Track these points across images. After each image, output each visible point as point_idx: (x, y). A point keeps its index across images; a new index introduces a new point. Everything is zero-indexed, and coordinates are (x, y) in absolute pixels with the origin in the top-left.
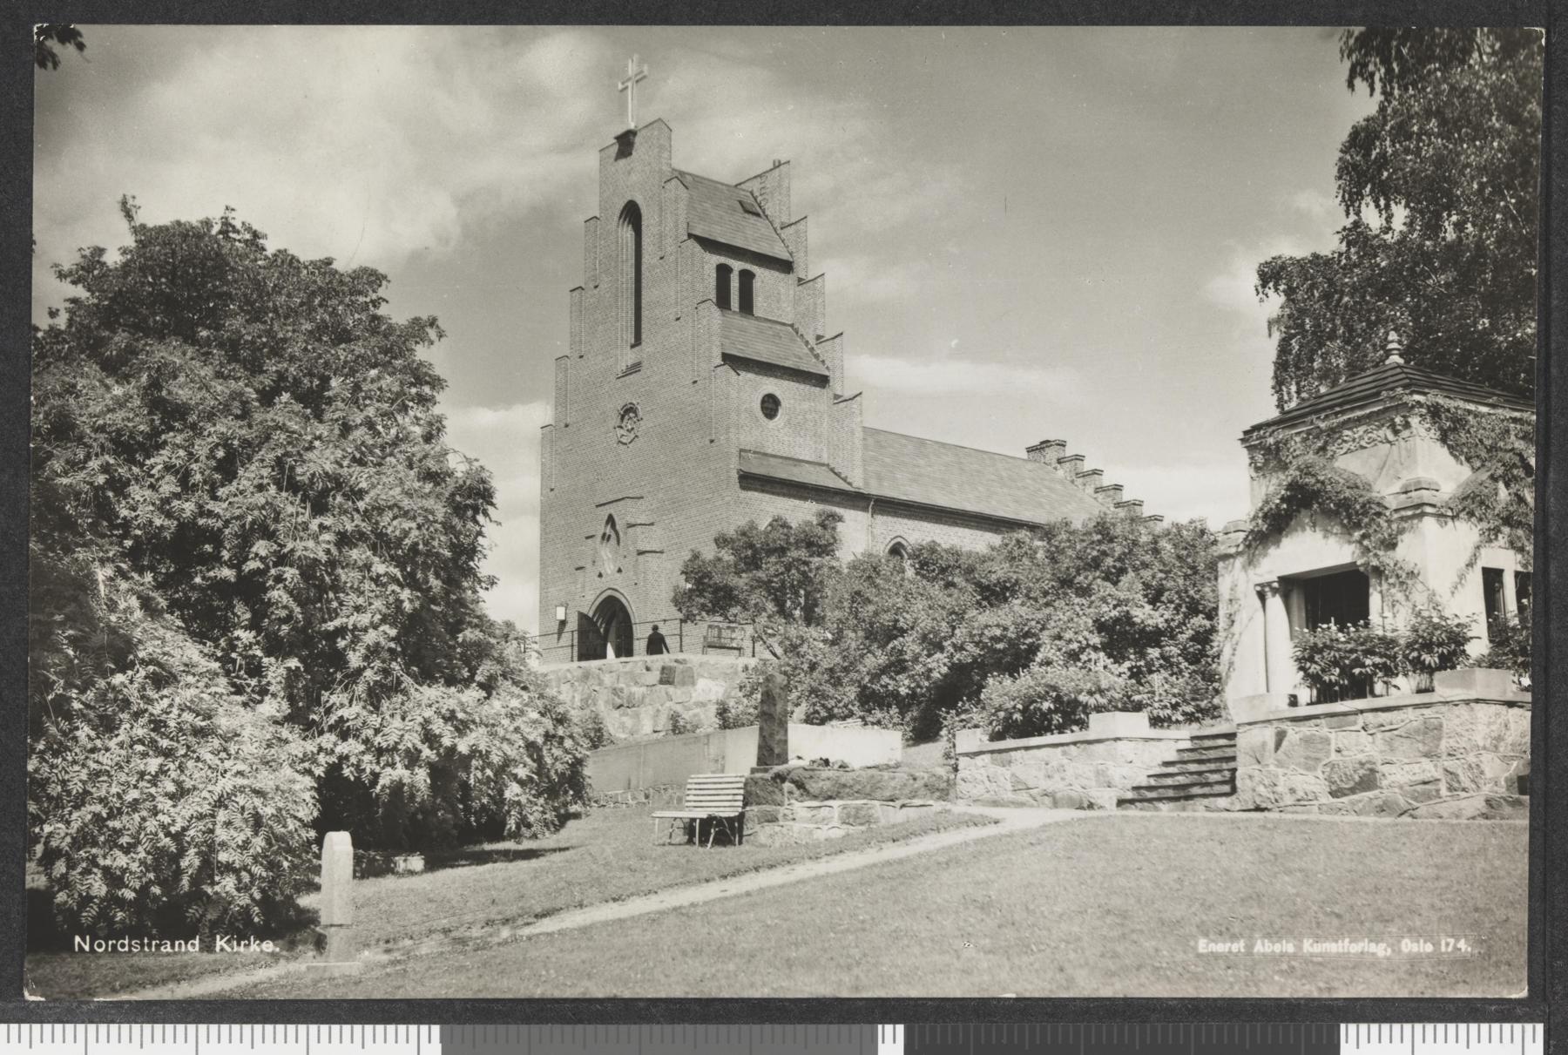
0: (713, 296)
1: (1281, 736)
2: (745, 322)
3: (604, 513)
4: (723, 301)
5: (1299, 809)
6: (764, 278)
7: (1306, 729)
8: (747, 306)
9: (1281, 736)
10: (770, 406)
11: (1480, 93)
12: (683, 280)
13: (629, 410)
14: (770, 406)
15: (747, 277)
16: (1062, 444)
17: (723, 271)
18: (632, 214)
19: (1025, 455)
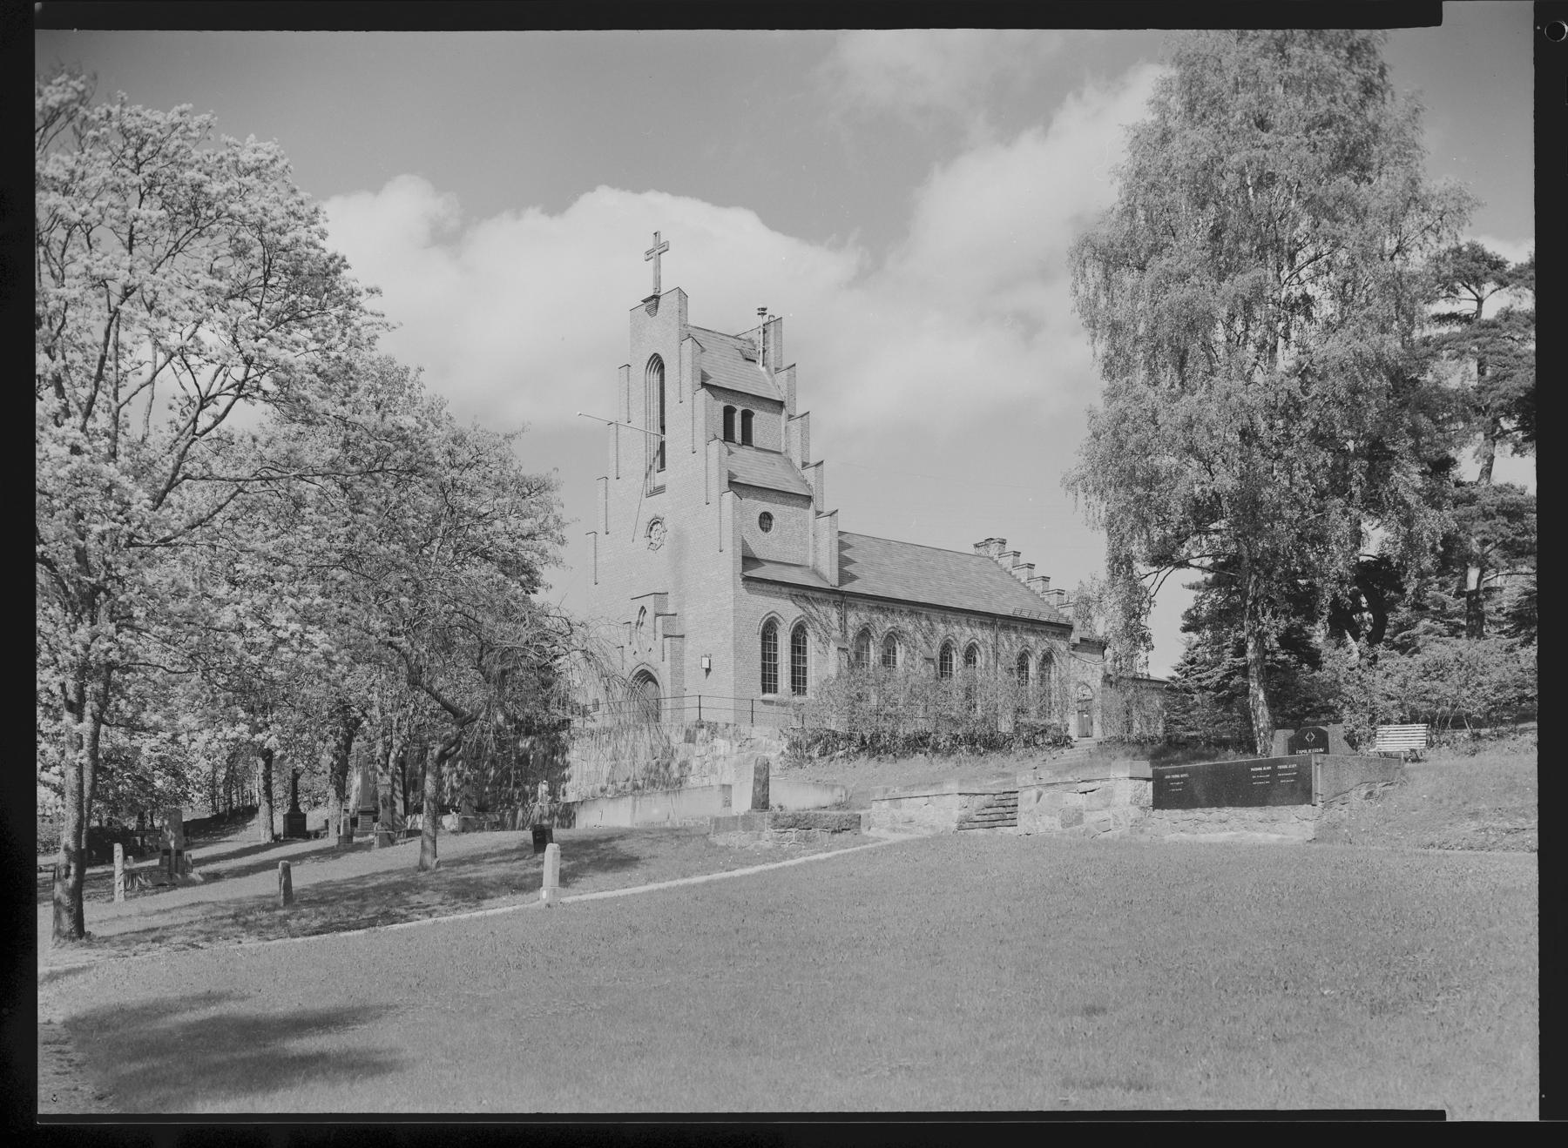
0: (721, 435)
1: (1040, 795)
2: (744, 452)
3: (638, 604)
4: (728, 436)
5: (158, 921)
6: (760, 418)
7: (1051, 790)
8: (747, 439)
9: (1040, 795)
10: (766, 520)
11: (499, 729)
12: (694, 417)
13: (656, 522)
14: (766, 520)
15: (747, 416)
16: (1003, 542)
17: (729, 412)
18: (657, 363)
19: (973, 551)
